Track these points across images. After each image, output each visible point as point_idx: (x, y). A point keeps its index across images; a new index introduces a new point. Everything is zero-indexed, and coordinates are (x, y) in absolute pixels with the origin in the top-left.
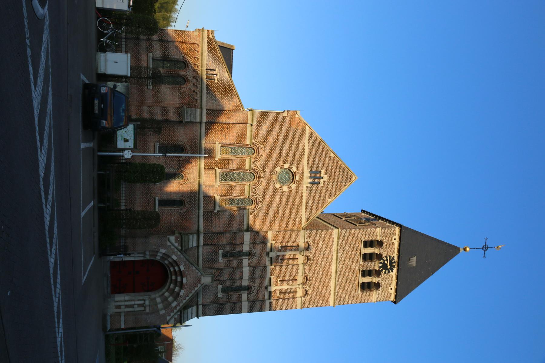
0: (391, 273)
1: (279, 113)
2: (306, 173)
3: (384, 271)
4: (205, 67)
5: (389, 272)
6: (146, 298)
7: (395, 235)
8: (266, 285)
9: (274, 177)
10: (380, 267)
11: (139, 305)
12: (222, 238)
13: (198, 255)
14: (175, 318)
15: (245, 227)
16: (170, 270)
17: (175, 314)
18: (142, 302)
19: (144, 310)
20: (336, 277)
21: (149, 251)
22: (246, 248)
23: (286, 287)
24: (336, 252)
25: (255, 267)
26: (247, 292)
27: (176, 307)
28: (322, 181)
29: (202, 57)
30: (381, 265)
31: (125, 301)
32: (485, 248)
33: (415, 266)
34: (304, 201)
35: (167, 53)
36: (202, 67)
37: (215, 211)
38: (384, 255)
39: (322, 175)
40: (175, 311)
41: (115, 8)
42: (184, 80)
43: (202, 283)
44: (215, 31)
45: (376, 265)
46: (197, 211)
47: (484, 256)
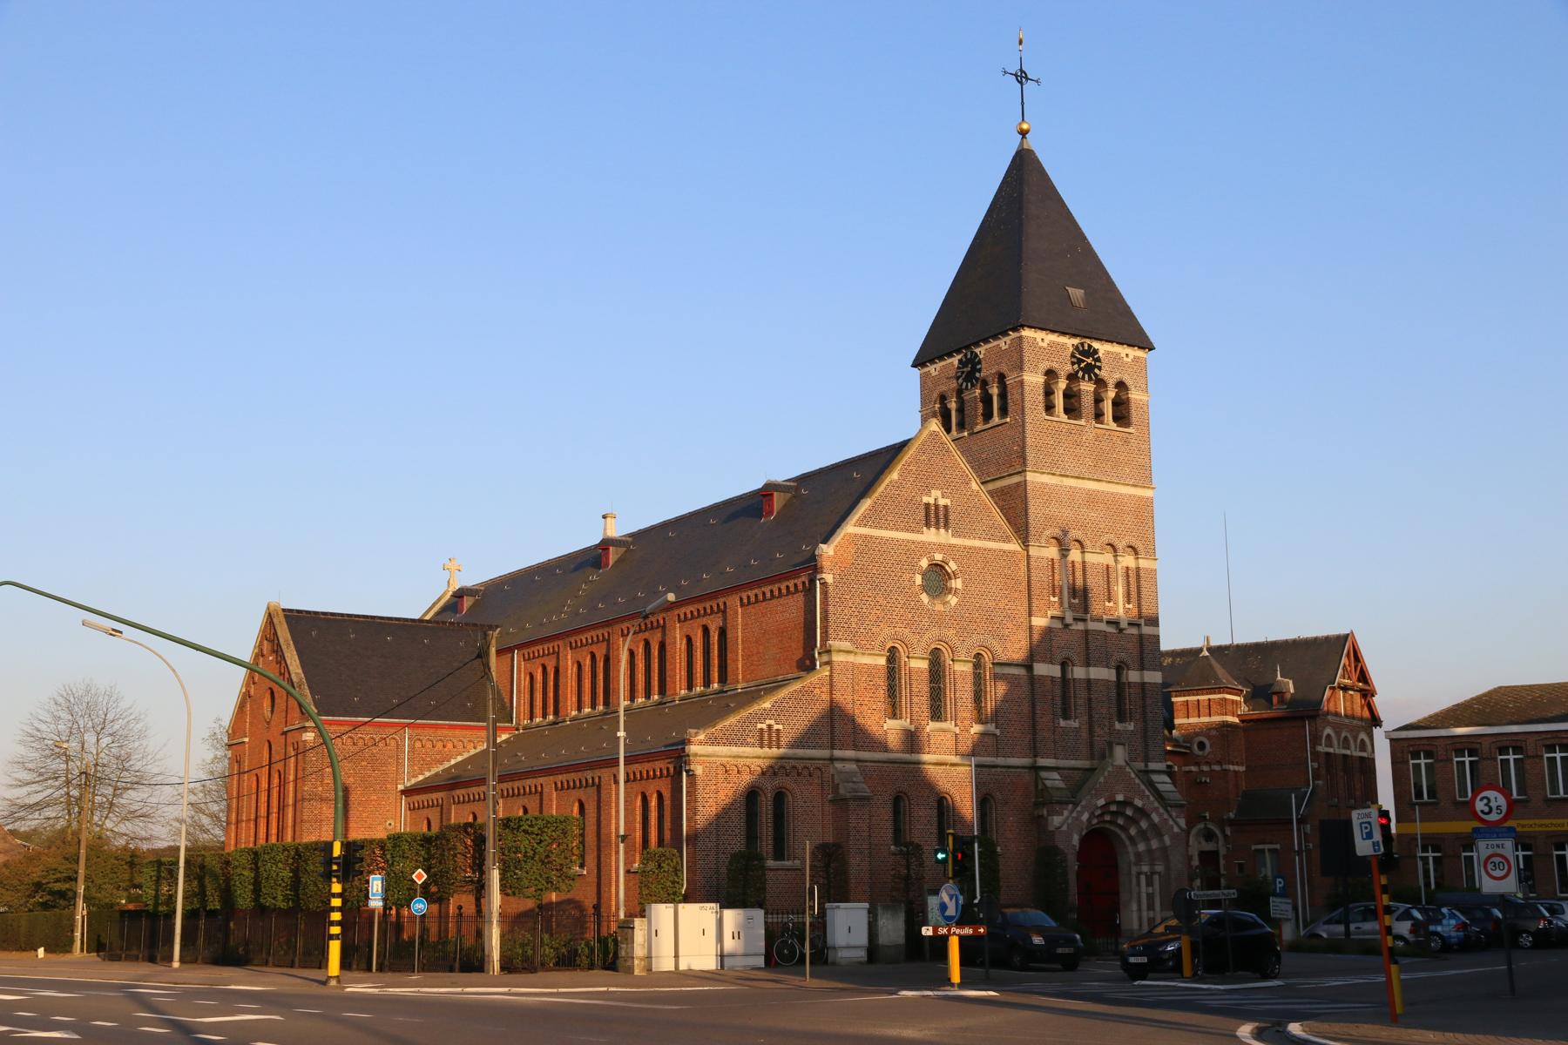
2: (931, 536)
4: (758, 751)
6: (1134, 870)
7: (1035, 339)
8: (1115, 631)
9: (939, 607)
11: (1150, 883)
12: (1043, 720)
13: (1069, 769)
14: (1177, 817)
15: (1021, 672)
16: (1107, 822)
17: (1171, 816)
18: (1143, 878)
19: (1160, 875)
20: (1106, 482)
22: (1056, 671)
23: (1119, 590)
24: (1064, 479)
25: (1088, 654)
26: (1125, 672)
27: (1160, 815)
28: (942, 502)
29: (741, 757)
30: (1086, 376)
31: (1140, 910)
32: (1021, 77)
33: (1083, 291)
34: (977, 543)
35: (737, 831)
36: (759, 757)
37: (998, 732)
38: (954, 384)
39: (932, 501)
40: (1166, 816)
41: (763, 932)
42: (779, 797)
43: (1124, 764)
46: (999, 769)
47: (1037, 81)
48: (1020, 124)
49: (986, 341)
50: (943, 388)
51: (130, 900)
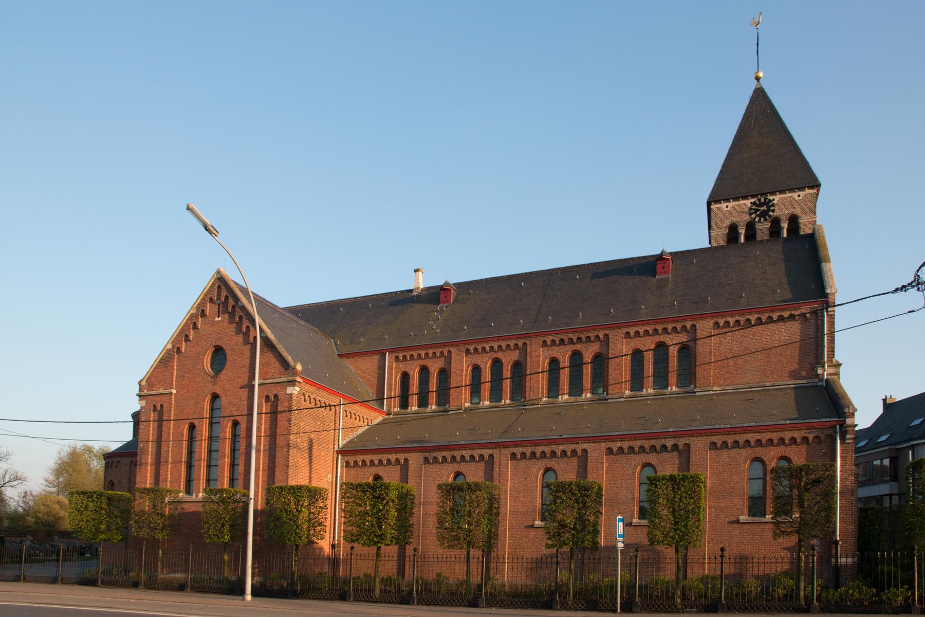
0: (775, 202)
1: (421, 572)
3: (771, 213)
5: (773, 205)
10: (765, 220)
21: (219, 305)
38: (747, 218)
44: (783, 292)
45: (763, 227)
48: (757, 73)
49: (782, 192)
50: (734, 219)
51: (203, 515)
